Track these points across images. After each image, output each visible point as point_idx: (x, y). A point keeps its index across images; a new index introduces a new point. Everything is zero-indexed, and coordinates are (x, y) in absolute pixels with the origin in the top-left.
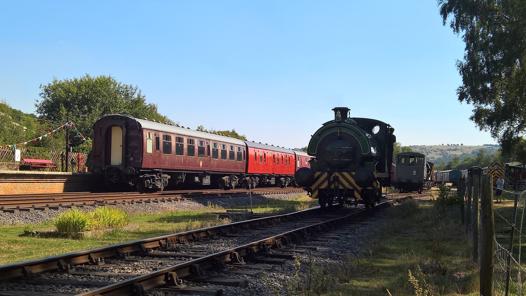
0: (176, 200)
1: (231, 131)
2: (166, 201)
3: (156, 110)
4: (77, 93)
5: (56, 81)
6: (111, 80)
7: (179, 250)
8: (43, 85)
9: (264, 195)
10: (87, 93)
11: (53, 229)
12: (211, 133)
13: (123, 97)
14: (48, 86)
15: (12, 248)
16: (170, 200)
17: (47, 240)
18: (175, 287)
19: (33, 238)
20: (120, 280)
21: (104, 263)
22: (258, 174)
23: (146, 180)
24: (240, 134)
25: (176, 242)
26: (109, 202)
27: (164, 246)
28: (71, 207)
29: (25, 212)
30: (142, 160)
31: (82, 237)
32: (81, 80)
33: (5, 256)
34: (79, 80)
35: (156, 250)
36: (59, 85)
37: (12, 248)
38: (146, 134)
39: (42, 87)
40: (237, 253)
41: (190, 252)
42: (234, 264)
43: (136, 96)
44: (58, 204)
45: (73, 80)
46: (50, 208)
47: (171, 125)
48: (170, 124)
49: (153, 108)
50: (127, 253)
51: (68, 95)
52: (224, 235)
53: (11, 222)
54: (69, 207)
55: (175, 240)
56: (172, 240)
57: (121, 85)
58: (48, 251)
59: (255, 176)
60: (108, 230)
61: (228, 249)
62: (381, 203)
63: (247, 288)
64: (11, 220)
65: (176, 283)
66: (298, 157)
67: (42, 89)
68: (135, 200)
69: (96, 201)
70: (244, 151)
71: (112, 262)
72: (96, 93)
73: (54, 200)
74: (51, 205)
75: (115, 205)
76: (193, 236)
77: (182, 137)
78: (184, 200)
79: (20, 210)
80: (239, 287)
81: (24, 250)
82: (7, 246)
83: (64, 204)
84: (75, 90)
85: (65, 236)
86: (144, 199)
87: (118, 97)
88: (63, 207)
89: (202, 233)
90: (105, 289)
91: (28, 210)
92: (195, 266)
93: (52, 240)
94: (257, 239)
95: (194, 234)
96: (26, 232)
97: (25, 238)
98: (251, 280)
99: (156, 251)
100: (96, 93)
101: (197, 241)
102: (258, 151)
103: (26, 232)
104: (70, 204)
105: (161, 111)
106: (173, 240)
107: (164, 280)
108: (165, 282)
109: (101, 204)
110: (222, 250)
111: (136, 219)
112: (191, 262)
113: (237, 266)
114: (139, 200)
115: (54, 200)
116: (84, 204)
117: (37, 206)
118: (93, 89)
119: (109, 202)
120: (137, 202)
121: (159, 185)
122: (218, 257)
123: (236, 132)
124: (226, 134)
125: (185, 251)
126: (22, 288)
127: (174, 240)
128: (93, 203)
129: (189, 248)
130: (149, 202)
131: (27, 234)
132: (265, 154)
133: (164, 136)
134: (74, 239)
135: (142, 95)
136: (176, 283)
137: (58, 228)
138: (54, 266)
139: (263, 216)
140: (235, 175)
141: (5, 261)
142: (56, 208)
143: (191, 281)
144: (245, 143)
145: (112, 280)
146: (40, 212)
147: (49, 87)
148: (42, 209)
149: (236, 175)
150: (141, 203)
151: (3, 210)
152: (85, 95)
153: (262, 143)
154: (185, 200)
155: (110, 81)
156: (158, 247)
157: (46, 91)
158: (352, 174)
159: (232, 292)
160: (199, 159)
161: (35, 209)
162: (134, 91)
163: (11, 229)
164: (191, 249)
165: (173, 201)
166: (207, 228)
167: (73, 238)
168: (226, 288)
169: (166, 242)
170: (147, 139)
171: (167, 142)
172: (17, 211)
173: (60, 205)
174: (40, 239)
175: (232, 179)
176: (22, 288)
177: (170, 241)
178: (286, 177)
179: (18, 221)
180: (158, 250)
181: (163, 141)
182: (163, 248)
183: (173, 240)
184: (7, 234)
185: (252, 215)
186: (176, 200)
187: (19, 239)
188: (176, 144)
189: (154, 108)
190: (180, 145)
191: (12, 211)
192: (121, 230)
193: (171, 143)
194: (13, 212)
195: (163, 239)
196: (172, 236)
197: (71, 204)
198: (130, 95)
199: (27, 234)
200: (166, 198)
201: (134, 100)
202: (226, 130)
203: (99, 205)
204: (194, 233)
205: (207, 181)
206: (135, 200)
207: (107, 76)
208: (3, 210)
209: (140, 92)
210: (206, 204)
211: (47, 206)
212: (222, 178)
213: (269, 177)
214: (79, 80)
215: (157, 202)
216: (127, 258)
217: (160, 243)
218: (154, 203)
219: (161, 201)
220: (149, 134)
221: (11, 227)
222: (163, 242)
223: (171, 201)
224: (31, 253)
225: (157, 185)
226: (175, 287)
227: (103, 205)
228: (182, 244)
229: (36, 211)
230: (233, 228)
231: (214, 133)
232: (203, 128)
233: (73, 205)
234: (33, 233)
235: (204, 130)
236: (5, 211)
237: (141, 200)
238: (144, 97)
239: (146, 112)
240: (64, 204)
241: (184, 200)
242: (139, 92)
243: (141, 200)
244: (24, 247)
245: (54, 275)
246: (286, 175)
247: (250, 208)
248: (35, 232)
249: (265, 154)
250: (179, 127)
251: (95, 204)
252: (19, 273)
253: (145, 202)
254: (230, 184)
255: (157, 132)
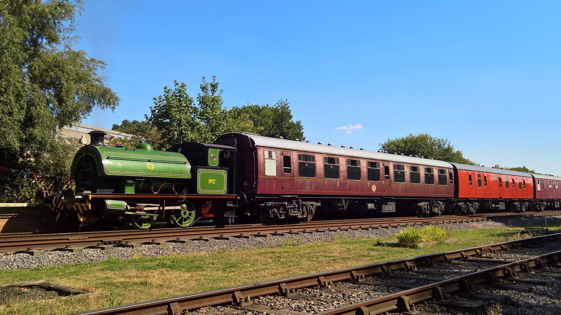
0: (483, 221)
1: (522, 167)
2: (475, 221)
3: (461, 155)
4: (404, 147)
5: (389, 140)
6: (428, 136)
7: (492, 257)
8: (381, 144)
9: (555, 216)
10: (411, 147)
11: (396, 241)
12: (505, 169)
13: (437, 147)
14: (384, 144)
15: (371, 254)
16: (478, 221)
17: (393, 248)
18: (407, 313)
19: (383, 247)
20: (451, 278)
21: (436, 265)
22: (475, 198)
23: (271, 210)
24: (530, 169)
25: (489, 251)
26: (432, 222)
27: (479, 254)
28: (406, 226)
29: (376, 230)
30: (257, 185)
31: (417, 247)
32: (407, 138)
33: (367, 259)
34: (405, 138)
35: (474, 257)
36: (392, 143)
37: (371, 254)
38: (262, 154)
39: (380, 145)
40: (541, 260)
41: (501, 259)
42: (541, 269)
43: (446, 146)
44: (397, 224)
45: (401, 139)
46: (392, 227)
47: (472, 165)
48: (472, 164)
49: (459, 154)
50: (453, 258)
51: (399, 149)
52: (527, 247)
53: (367, 237)
54: (404, 226)
55: (488, 249)
56: (485, 250)
57: (436, 139)
58: (395, 256)
59: (471, 202)
60: (435, 242)
61: (532, 257)
62: (484, 269)
63: (553, 287)
64: (367, 235)
65: (513, 276)
66: (538, 181)
67: (380, 146)
68: (452, 221)
69: (423, 222)
70: (451, 174)
71: (442, 264)
72: (417, 146)
73: (394, 221)
74: (392, 225)
75: (437, 224)
76: (426, 261)
77: (312, 154)
78: (489, 220)
79: (373, 228)
80: (546, 287)
81: (378, 255)
82: (367, 252)
83: (401, 224)
84: (403, 145)
85: (405, 246)
86: (458, 220)
87: (434, 147)
88: (400, 226)
89: (392, 265)
90: (425, 288)
91: (378, 228)
92: (465, 282)
93: (396, 249)
94: (555, 250)
95: (385, 267)
96: (378, 243)
97: (378, 247)
98: (556, 281)
99: (474, 258)
100: (417, 146)
101: (505, 251)
102: (527, 179)
103: (378, 243)
104: (413, 223)
105: (465, 156)
106: (486, 250)
107: (396, 305)
108: (503, 275)
109: (427, 224)
110: (527, 258)
111: (453, 235)
112: (486, 271)
113: (542, 270)
114: (454, 221)
115: (394, 221)
116: (415, 224)
117: (383, 225)
118: (415, 144)
119: (432, 222)
120: (453, 223)
121: (472, 209)
122: (491, 272)
123: (527, 168)
124: (518, 169)
125: (497, 258)
126: (383, 280)
127: (487, 249)
128: (421, 223)
129: (500, 256)
130: (462, 222)
131: (379, 244)
132: (524, 181)
133: (394, 166)
134: (411, 248)
135: (451, 145)
136: (513, 276)
137: (400, 241)
138: (203, 304)
139: (558, 232)
140: (439, 200)
141: (367, 262)
142: (396, 227)
143: (505, 280)
144: (532, 175)
145: (445, 277)
146: (385, 230)
147: (385, 144)
148: (387, 228)
149: (441, 201)
150: (456, 223)
151: (362, 228)
152: (410, 148)
153: (485, 166)
154: (490, 220)
155: (427, 137)
156: (475, 255)
157: (383, 147)
158: (14, 169)
159: (541, 290)
160: (369, 183)
161: (382, 227)
162: (444, 143)
163: (368, 241)
164: (501, 256)
165: (480, 221)
166: (523, 239)
167: (411, 247)
168: (535, 286)
169: (481, 251)
170: (264, 159)
171: (307, 163)
172: (370, 229)
173: (398, 225)
174: (388, 248)
175: (433, 205)
176: (383, 280)
177: (484, 250)
178: (521, 201)
179: (372, 235)
180: (475, 257)
181: (368, 168)
182: (479, 255)
183: (486, 250)
184: (366, 244)
185: (547, 232)
186: (483, 220)
187: (374, 247)
188: (425, 174)
189: (460, 154)
190: (307, 165)
191: (367, 229)
192: (444, 242)
193: (315, 164)
194: (368, 229)
195: (478, 249)
196: (485, 247)
197: (405, 224)
198: (442, 146)
199: (379, 244)
200: (475, 219)
201: (445, 149)
202: (518, 167)
203: (425, 225)
204: (383, 265)
205: (502, 206)
206: (452, 221)
207: (425, 134)
208: (362, 228)
209: (450, 143)
210: (507, 225)
211: (390, 225)
212: (418, 204)
213: (496, 201)
214: (405, 138)
215: (468, 222)
216: (453, 262)
217: (476, 252)
218: (466, 223)
219: (471, 221)
220: (556, 182)
221: (368, 239)
222: (479, 251)
223: (479, 221)
224: (384, 257)
225: (470, 210)
226: (407, 313)
227: (428, 225)
228: (493, 252)
229: (383, 229)
230: (524, 242)
231: (508, 169)
232: (499, 166)
233: (407, 224)
234: (383, 244)
235: (500, 167)
236: (362, 229)
237: (456, 221)
238: (453, 146)
239: (455, 157)
240: (401, 224)
241: (489, 220)
242: (448, 143)
243: (456, 221)
244: (378, 253)
245: (403, 272)
246: (522, 199)
247: (546, 227)
248: (384, 243)
249: (524, 181)
250: (344, 147)
251: (422, 224)
252: (379, 270)
253: (459, 222)
254: (521, 208)
255: (284, 150)
